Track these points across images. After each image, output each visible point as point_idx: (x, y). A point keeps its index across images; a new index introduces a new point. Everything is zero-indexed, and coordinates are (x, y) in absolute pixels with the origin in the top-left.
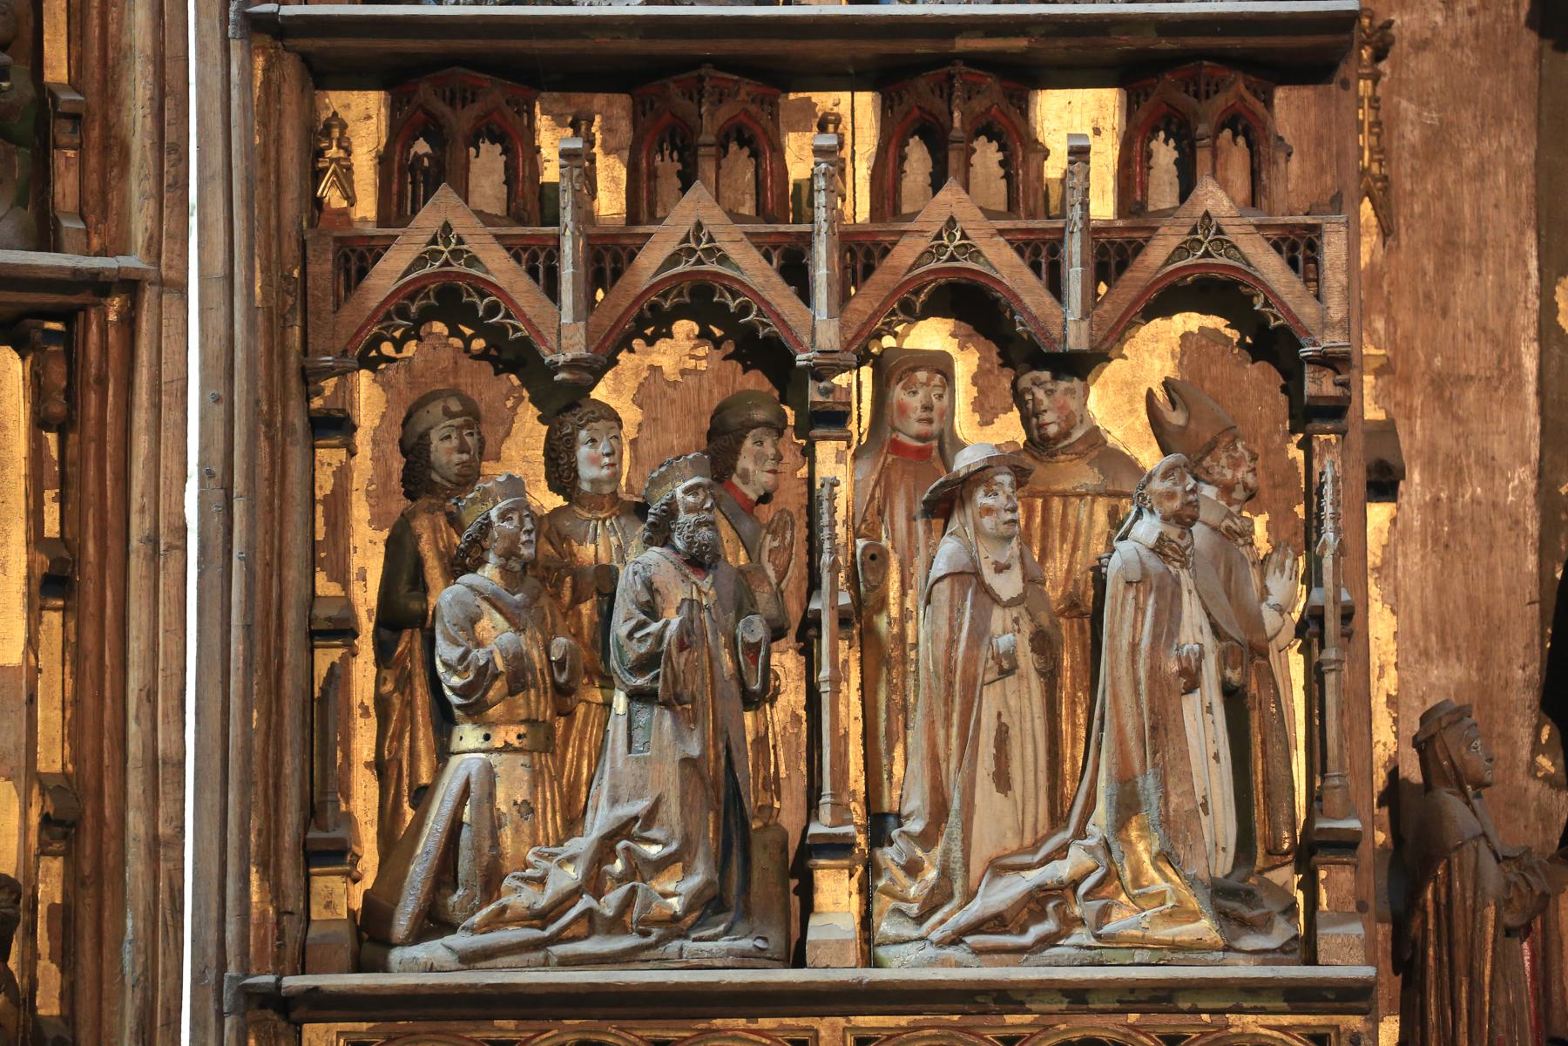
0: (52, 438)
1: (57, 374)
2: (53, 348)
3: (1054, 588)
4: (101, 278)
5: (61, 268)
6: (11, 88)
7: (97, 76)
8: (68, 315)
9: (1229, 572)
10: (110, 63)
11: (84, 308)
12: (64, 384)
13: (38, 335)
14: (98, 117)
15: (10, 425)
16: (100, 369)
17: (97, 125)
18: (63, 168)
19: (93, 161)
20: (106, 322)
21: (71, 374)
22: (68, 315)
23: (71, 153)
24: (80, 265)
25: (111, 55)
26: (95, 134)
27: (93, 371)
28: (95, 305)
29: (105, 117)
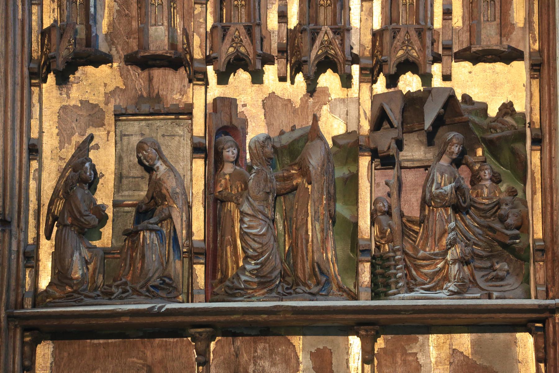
0: (542, 365)
1: (541, 340)
2: (539, 333)
3: (448, 143)
4: (549, 308)
5: (534, 305)
6: (519, 242)
7: (550, 235)
8: (543, 321)
9: (291, 227)
10: (555, 230)
11: (547, 318)
12: (543, 345)
13: (533, 329)
14: (551, 250)
15: (530, 361)
16: (554, 340)
17: (550, 252)
18: (539, 269)
19: (549, 266)
20: (555, 323)
21: (545, 343)
22: (543, 321)
23: (541, 263)
24: (541, 303)
25: (554, 227)
26: (550, 255)
27: (551, 341)
28: (550, 317)
29: (553, 250)
